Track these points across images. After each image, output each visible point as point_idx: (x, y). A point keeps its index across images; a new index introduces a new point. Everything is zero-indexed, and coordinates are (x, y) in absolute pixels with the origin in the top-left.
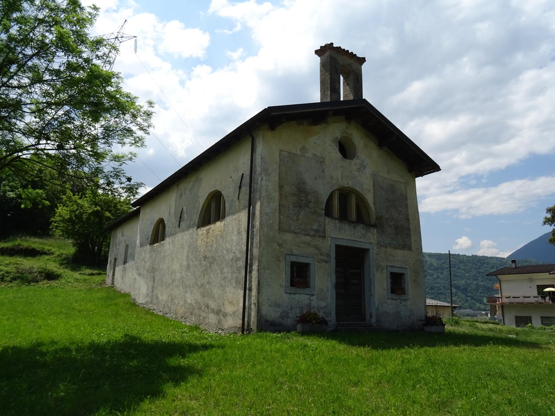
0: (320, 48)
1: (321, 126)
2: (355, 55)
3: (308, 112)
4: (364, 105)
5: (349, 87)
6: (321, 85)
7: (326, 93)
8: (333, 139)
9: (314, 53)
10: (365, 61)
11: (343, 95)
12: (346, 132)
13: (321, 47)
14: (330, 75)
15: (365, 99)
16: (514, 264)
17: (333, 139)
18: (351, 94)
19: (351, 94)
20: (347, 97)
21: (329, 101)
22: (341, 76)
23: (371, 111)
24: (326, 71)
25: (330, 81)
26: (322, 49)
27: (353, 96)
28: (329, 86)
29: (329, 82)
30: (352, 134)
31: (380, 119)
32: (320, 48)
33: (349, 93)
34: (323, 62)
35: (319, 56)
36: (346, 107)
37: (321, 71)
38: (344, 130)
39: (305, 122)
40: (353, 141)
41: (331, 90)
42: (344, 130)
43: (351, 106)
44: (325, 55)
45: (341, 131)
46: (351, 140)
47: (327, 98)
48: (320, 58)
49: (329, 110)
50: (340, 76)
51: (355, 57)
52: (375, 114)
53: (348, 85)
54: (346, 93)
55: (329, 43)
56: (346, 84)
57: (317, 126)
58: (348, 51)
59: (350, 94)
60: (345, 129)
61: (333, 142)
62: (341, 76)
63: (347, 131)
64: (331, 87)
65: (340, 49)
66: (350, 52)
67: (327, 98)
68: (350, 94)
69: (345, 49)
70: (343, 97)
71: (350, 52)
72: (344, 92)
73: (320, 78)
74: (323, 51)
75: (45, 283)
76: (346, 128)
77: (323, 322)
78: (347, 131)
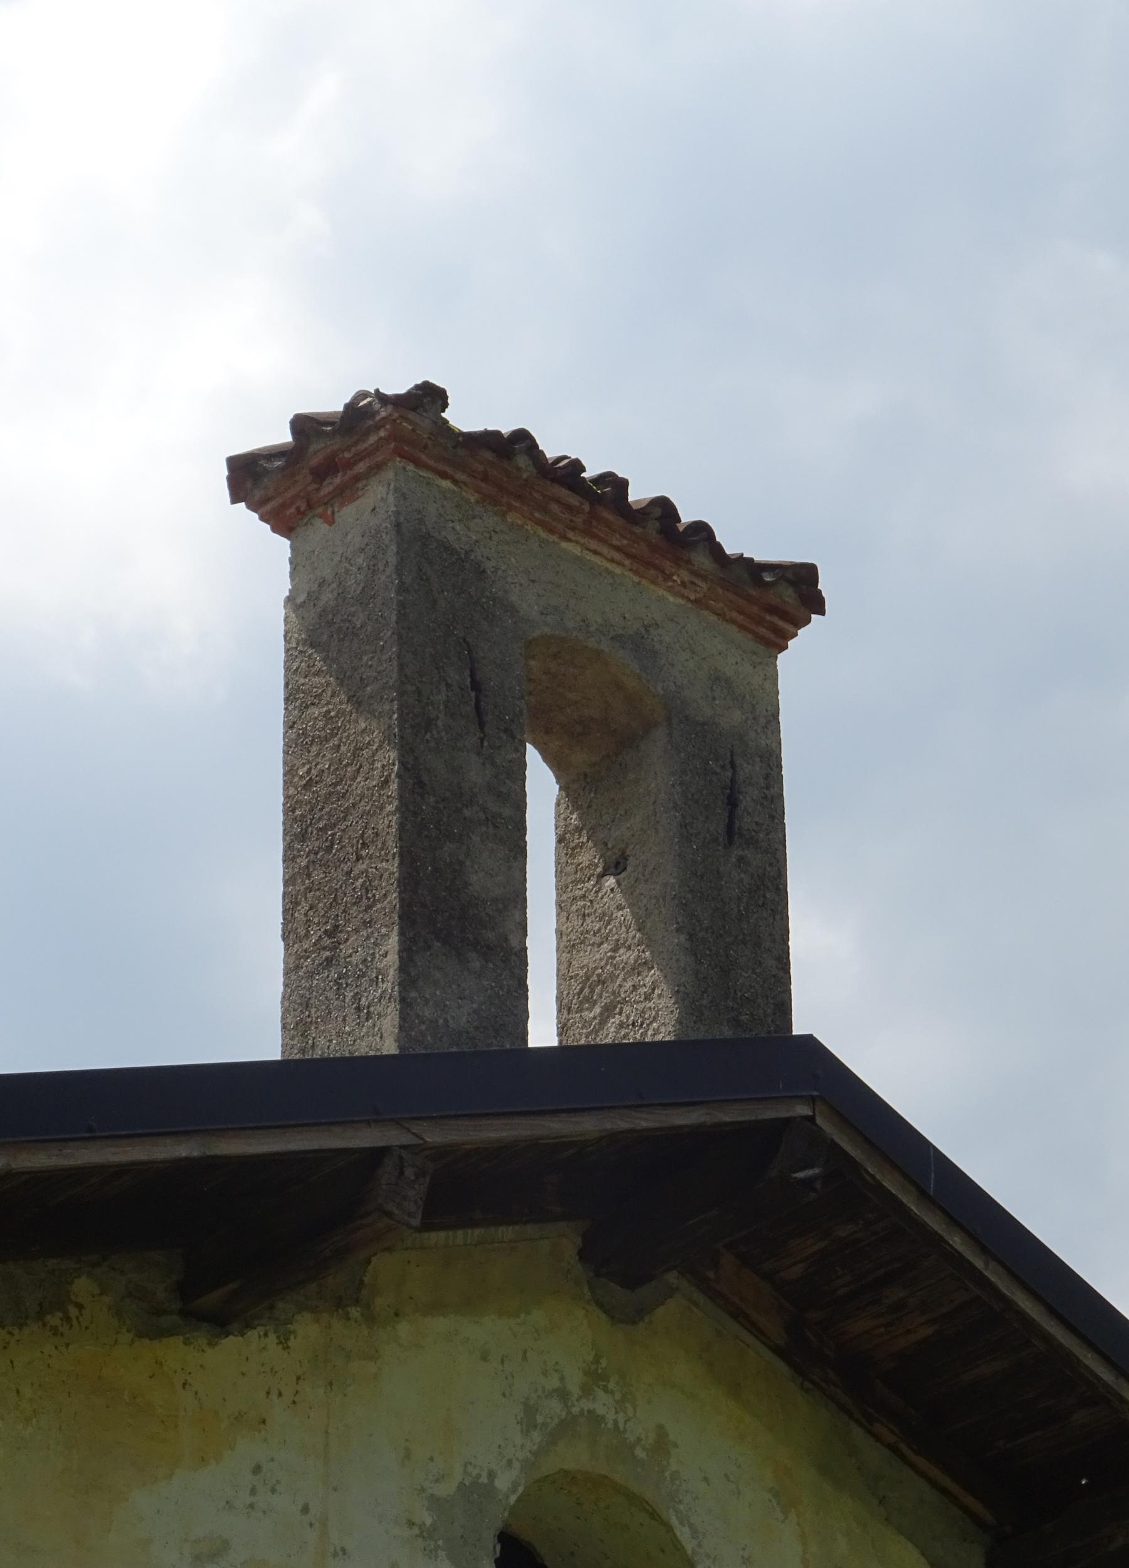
0: (285, 437)
1: (284, 1342)
2: (702, 530)
3: (121, 1170)
4: (803, 1110)
5: (629, 892)
6: (289, 858)
7: (353, 950)
8: (435, 1502)
9: (228, 455)
10: (817, 605)
11: (563, 977)
12: (594, 1419)
13: (303, 425)
14: (407, 751)
15: (810, 1044)
16: (373, 1258)
17: (435, 1502)
18: (655, 973)
19: (655, 973)
20: (609, 1010)
21: (390, 1047)
22: (532, 755)
23: (891, 1183)
24: (356, 701)
25: (408, 810)
26: (318, 451)
27: (681, 995)
28: (394, 866)
29: (388, 821)
30: (662, 1444)
31: (995, 1276)
32: (285, 437)
33: (626, 956)
34: (327, 597)
35: (282, 523)
36: (589, 1126)
37: (291, 696)
38: (562, 1394)
39: (82, 1286)
40: (683, 1534)
41: (408, 919)
42: (562, 1394)
43: (645, 1121)
44: (348, 513)
45: (530, 1410)
46: (654, 1515)
47: (364, 1013)
48: (282, 546)
49: (381, 1153)
50: (523, 766)
51: (702, 559)
52: (934, 1222)
53: (616, 866)
54: (590, 958)
55: (398, 385)
56: (588, 857)
57: (231, 1343)
58: (616, 485)
59: (638, 968)
60: (574, 1381)
61: (426, 1533)
62: (532, 755)
63: (602, 1404)
64: (409, 881)
65: (522, 461)
66: (636, 494)
67: (364, 1013)
68: (638, 968)
69: (577, 466)
70: (563, 1006)
71: (636, 494)
72: (568, 945)
73: (290, 772)
74: (321, 474)
75: (602, 992)
76: (595, 1377)
77: (277, 455)
78: (602, 1404)
